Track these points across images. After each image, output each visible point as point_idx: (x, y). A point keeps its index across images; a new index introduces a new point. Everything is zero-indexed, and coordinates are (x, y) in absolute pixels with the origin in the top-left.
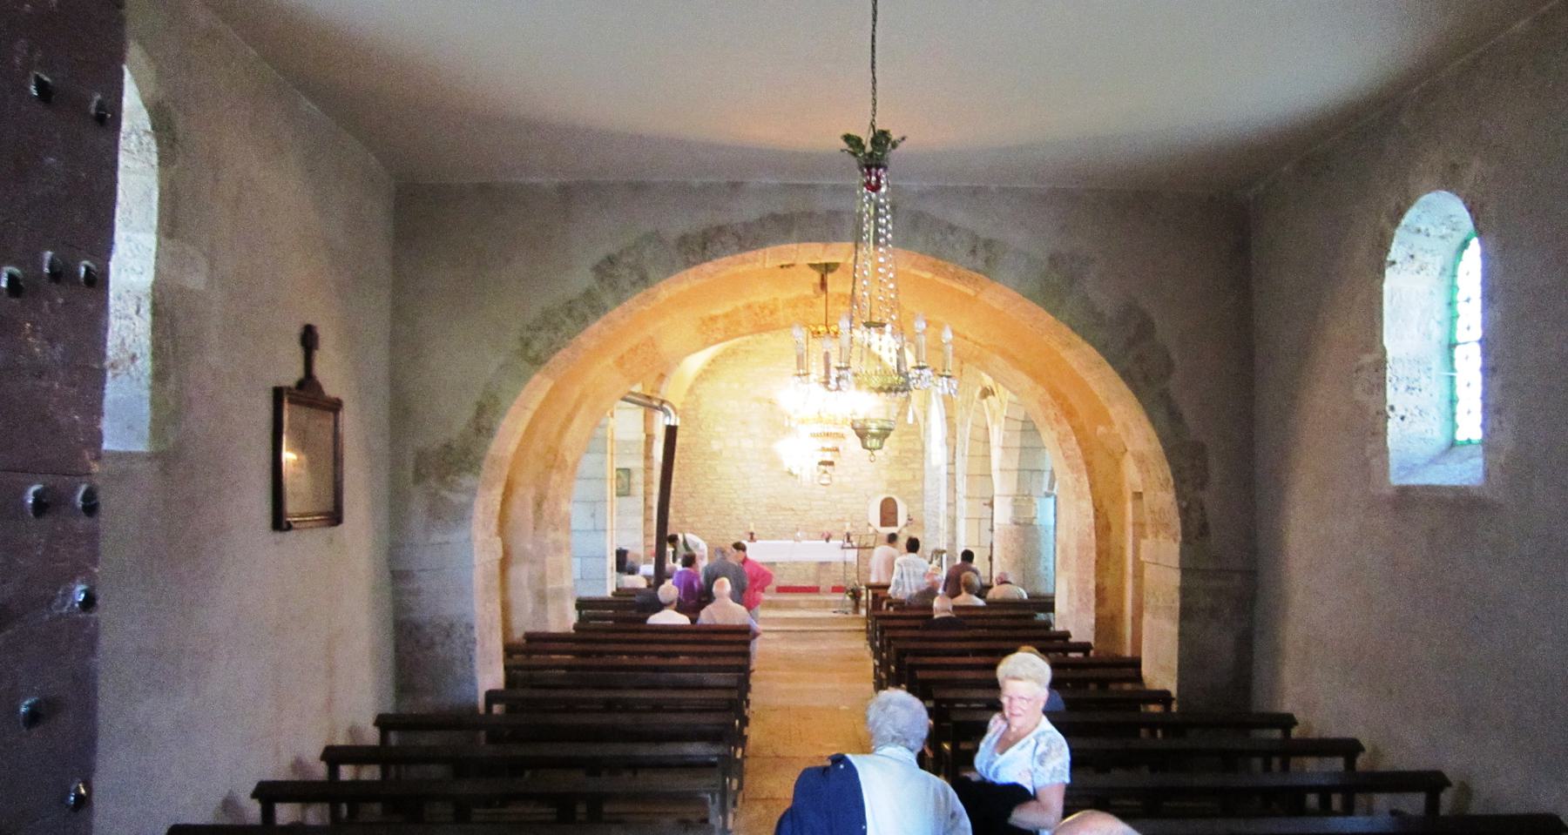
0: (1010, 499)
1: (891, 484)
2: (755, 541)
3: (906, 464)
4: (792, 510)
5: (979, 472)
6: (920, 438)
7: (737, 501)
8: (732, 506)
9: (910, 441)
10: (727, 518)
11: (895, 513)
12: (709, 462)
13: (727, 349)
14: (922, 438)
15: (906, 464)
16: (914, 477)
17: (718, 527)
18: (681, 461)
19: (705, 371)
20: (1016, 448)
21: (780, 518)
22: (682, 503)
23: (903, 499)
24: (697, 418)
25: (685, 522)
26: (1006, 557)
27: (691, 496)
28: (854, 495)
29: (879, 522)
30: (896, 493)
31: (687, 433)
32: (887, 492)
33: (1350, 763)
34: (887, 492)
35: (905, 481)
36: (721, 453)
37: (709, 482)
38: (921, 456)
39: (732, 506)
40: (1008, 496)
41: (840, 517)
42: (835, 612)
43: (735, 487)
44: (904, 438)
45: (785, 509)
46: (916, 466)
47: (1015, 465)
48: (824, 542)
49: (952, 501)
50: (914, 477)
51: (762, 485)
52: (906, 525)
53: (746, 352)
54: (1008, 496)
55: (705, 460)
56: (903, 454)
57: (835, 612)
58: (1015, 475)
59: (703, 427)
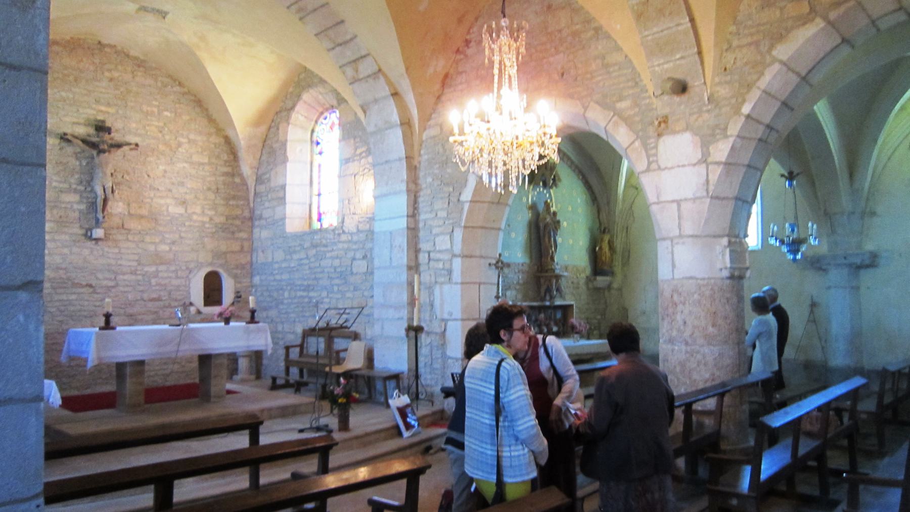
1: (217, 255)
2: (114, 328)
4: (91, 286)
5: (480, 224)
6: (249, 204)
9: (237, 206)
11: (219, 289)
14: (252, 205)
15: (233, 233)
16: (242, 247)
20: (744, 165)
21: (73, 297)
23: (228, 271)
29: (203, 304)
30: (221, 266)
32: (211, 264)
33: (254, 439)
34: (211, 264)
35: (233, 252)
38: (250, 224)
41: (154, 296)
42: (301, 431)
44: (231, 202)
45: (82, 286)
46: (243, 235)
48: (223, 324)
49: (413, 264)
50: (242, 247)
52: (233, 304)
57: (301, 431)
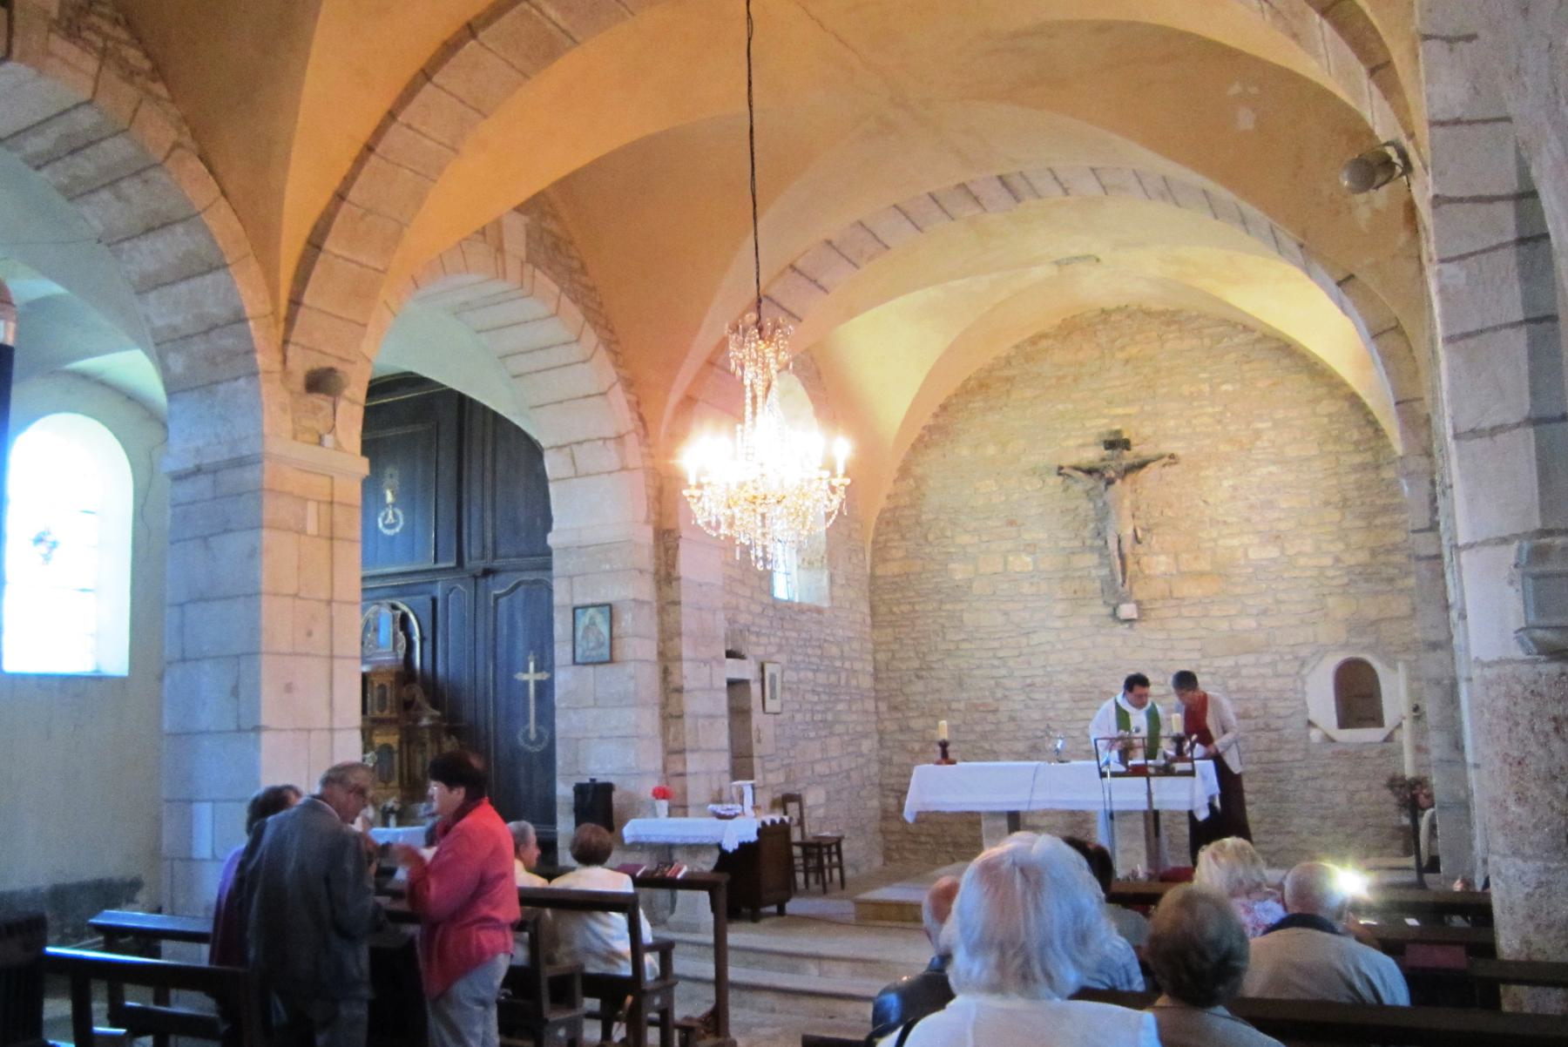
0: (1510, 553)
3: (1391, 580)
7: (1007, 682)
8: (999, 694)
10: (991, 717)
12: (948, 607)
13: (969, 379)
17: (972, 737)
18: (895, 609)
19: (929, 429)
22: (901, 690)
24: (918, 523)
25: (909, 729)
26: (1521, 799)
27: (919, 677)
28: (1267, 658)
31: (901, 554)
32: (1346, 646)
34: (1346, 646)
36: (970, 587)
37: (952, 647)
39: (999, 694)
40: (1504, 541)
43: (1001, 654)
47: (1519, 404)
51: (1059, 646)
53: (1008, 379)
54: (1504, 541)
55: (941, 602)
56: (1382, 558)
58: (1526, 441)
59: (931, 537)
